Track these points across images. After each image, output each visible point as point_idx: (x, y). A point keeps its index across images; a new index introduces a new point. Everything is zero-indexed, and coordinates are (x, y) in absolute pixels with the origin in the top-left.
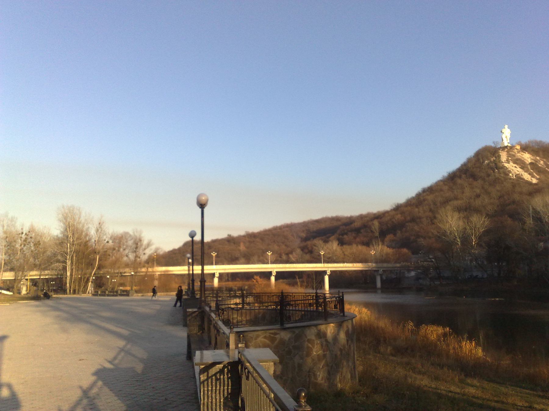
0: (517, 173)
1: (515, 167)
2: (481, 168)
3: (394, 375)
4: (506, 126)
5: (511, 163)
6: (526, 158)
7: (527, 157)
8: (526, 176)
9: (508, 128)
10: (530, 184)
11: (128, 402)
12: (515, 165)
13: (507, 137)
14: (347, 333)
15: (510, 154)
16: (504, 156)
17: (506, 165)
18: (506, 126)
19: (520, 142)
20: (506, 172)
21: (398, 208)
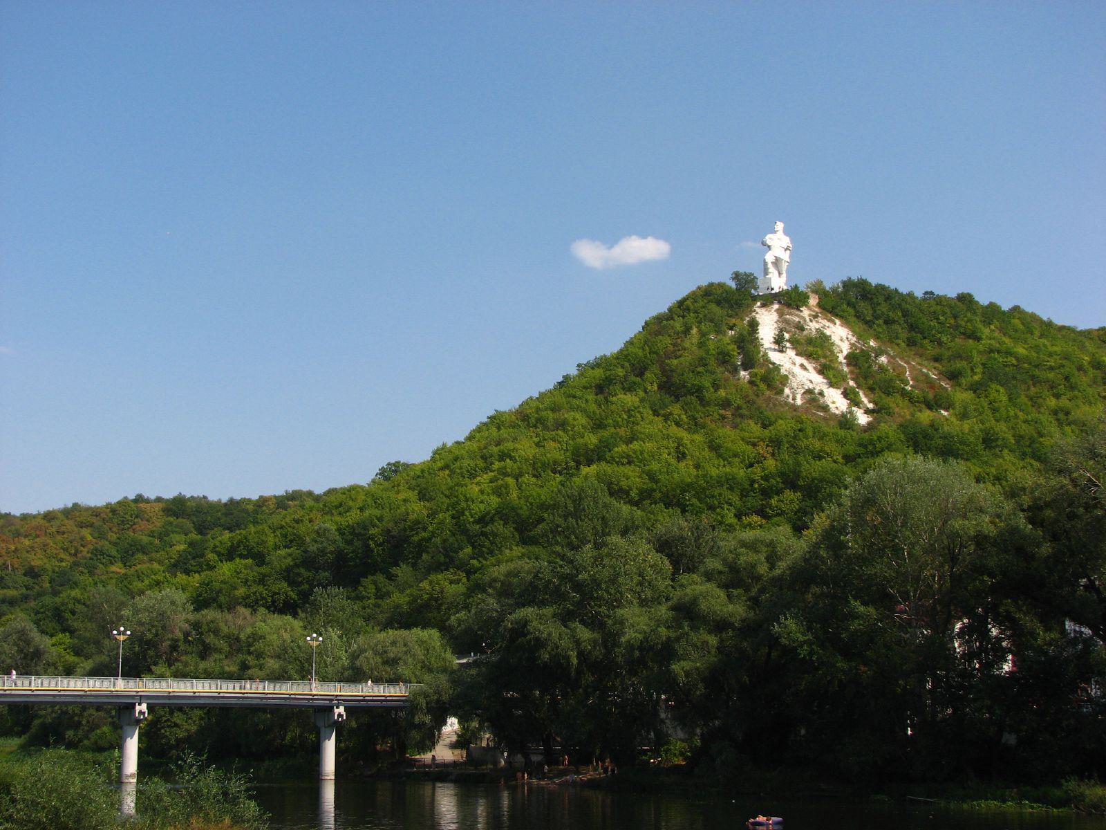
0: (809, 385)
1: (802, 366)
2: (691, 353)
3: (591, 773)
4: (780, 226)
5: (791, 353)
6: (835, 339)
7: (841, 336)
8: (836, 401)
9: (786, 232)
10: (846, 422)
11: (113, 751)
12: (800, 360)
13: (778, 258)
14: (853, 379)
15: (787, 322)
16: (767, 323)
17: (775, 357)
18: (780, 226)
19: (820, 283)
20: (772, 379)
21: (25, 517)
